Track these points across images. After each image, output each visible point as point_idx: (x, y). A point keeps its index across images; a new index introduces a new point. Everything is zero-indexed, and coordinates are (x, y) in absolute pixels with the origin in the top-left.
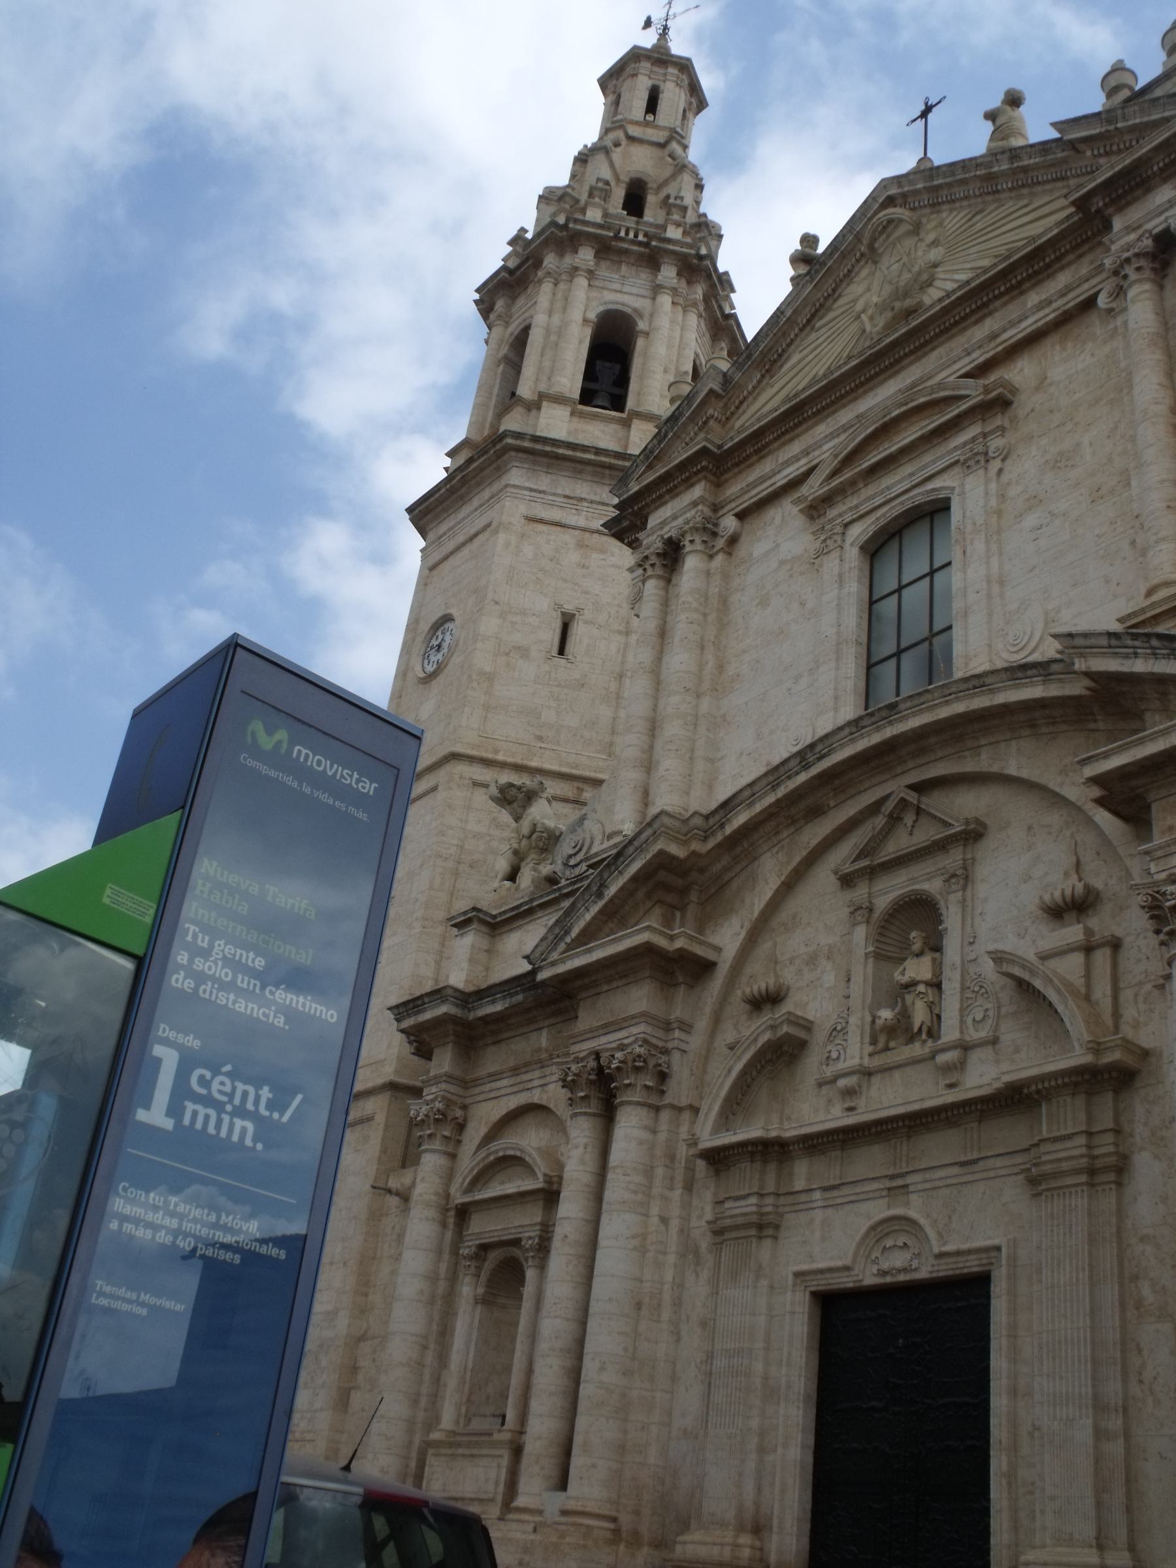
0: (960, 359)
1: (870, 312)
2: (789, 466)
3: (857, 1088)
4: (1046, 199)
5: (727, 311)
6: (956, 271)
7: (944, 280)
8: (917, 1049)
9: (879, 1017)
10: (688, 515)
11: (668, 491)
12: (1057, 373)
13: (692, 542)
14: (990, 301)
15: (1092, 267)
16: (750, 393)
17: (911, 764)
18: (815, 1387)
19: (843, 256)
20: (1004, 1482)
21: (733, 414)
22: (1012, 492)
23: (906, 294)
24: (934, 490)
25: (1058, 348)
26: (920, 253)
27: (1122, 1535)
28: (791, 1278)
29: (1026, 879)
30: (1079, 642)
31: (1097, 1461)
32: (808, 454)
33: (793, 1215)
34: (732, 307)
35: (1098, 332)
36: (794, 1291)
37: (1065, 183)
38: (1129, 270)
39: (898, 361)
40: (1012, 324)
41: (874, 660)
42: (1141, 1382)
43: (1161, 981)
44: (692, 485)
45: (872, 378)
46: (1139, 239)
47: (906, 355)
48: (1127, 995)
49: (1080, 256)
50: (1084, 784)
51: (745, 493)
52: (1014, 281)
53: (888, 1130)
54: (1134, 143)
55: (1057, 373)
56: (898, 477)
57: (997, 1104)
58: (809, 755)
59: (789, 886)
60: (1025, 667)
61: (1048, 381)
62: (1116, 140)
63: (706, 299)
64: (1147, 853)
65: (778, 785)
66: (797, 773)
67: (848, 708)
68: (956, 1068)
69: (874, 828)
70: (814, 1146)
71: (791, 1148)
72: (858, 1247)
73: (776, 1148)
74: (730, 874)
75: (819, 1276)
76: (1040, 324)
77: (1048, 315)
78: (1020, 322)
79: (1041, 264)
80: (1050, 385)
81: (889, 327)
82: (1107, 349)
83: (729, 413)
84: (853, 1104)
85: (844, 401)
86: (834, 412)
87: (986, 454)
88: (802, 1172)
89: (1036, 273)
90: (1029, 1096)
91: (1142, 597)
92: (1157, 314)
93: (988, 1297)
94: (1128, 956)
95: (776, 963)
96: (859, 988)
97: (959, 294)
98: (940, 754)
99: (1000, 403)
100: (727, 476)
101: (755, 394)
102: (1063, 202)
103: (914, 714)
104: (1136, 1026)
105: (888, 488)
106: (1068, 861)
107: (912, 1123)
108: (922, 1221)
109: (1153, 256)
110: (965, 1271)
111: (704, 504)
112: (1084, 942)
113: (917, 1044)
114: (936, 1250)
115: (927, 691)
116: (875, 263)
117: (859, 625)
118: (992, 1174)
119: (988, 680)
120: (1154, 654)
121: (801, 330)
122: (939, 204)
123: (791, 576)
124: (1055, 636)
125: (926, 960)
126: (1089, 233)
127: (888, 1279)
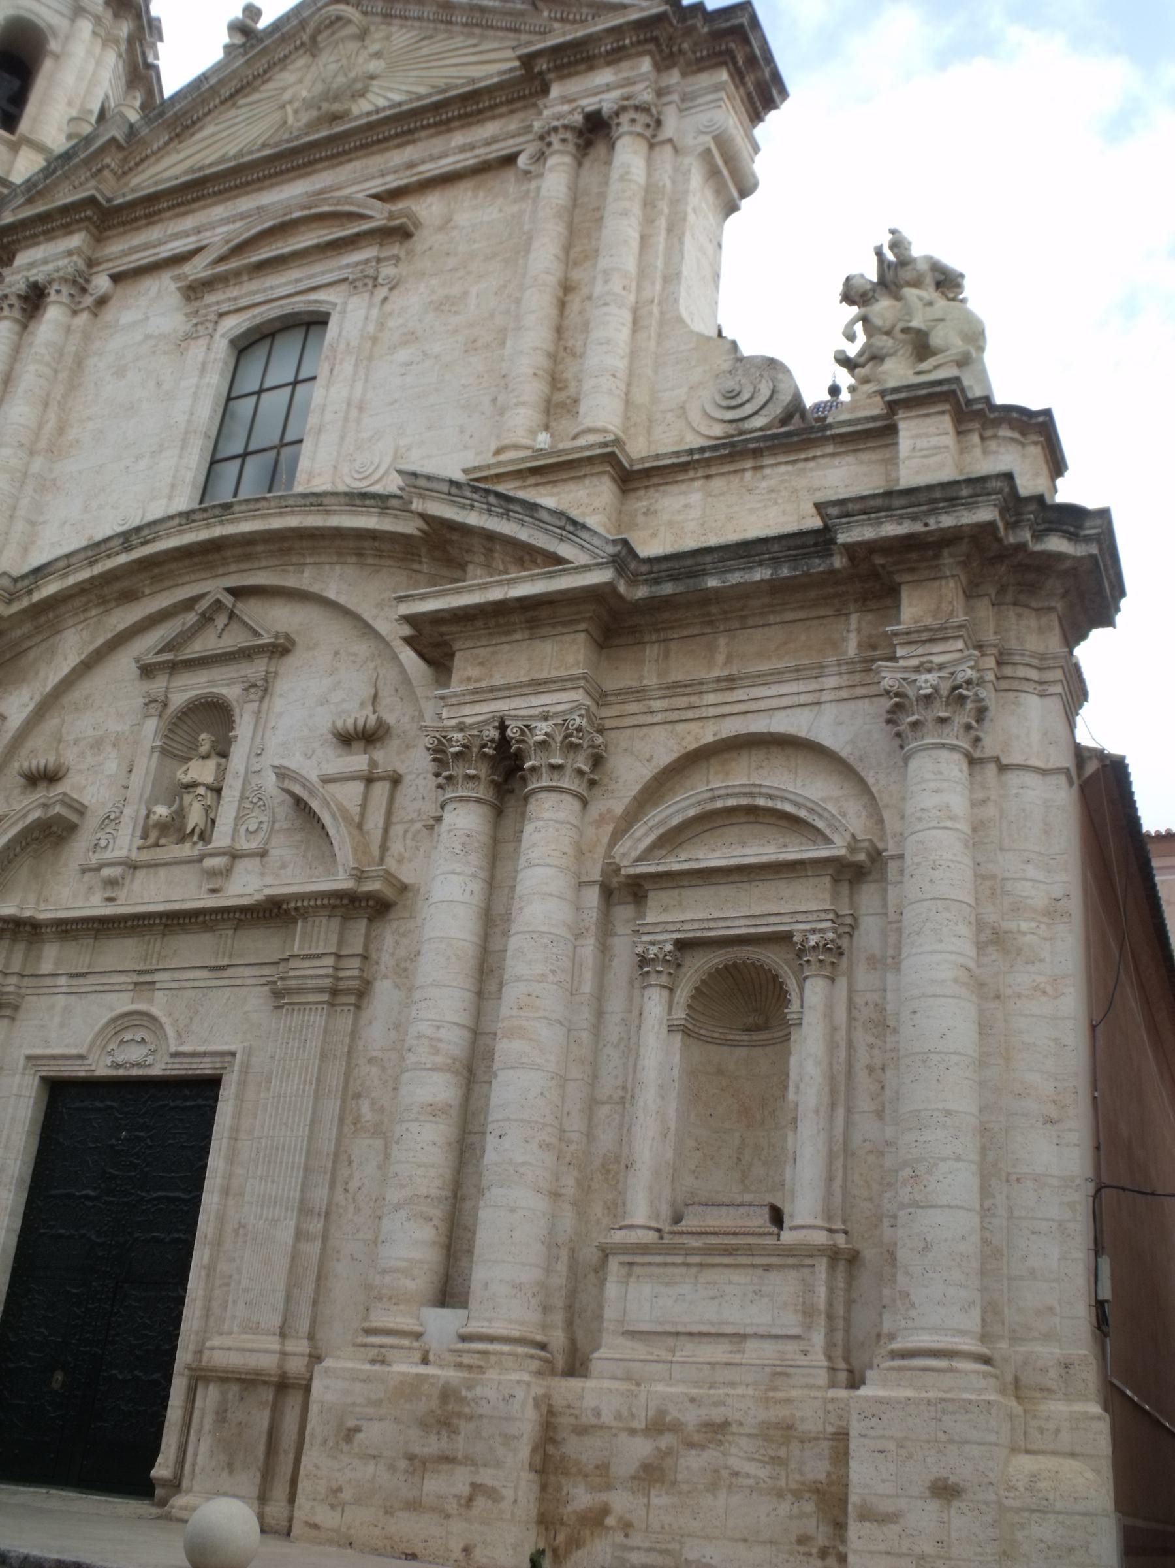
0: (373, 178)
1: (296, 105)
2: (177, 239)
3: (120, 880)
4: (496, 45)
5: (151, 59)
6: (391, 89)
7: (378, 95)
8: (187, 850)
9: (154, 813)
10: (61, 263)
11: (45, 233)
12: (463, 218)
13: (58, 292)
14: (416, 129)
15: (522, 125)
16: (153, 153)
17: (233, 568)
18: (30, 1171)
19: (284, 39)
20: (203, 1273)
21: (131, 169)
22: (391, 323)
23: (336, 98)
24: (316, 301)
25: (470, 194)
26: (360, 60)
27: (304, 1326)
28: (22, 1061)
29: (324, 701)
30: (422, 482)
31: (293, 1258)
32: (199, 232)
33: (35, 998)
34: (157, 57)
35: (511, 190)
36: (23, 1074)
37: (517, 36)
38: (554, 139)
39: (311, 163)
40: (432, 159)
41: (219, 456)
42: (346, 1190)
43: (432, 822)
44: (71, 233)
45: (282, 172)
46: (571, 112)
47: (321, 160)
48: (397, 830)
49: (512, 112)
50: (397, 620)
51: (126, 255)
52: (444, 117)
53: (138, 926)
54: (590, 18)
55: (463, 218)
56: (284, 280)
57: (255, 915)
58: (134, 537)
59: (87, 666)
60: (364, 496)
61: (452, 224)
62: (574, 10)
63: (131, 40)
64: (442, 698)
65: (96, 561)
66: (118, 554)
67: (182, 499)
68: (221, 873)
69: (184, 624)
70: (66, 931)
71: (43, 930)
72: (98, 1035)
73: (28, 928)
74: (30, 643)
75: (52, 1062)
76: (459, 166)
77: (468, 160)
78: (440, 158)
79: (474, 107)
80: (452, 228)
81: (313, 126)
82: (515, 208)
83: (126, 168)
84: (113, 895)
85: (248, 188)
86: (236, 197)
87: (376, 279)
88: (51, 956)
89: (467, 115)
90: (287, 912)
91: (491, 454)
92: (570, 188)
93: (216, 1100)
94: (406, 792)
95: (60, 741)
96: (140, 781)
97: (388, 113)
98: (264, 563)
99: (401, 233)
100: (109, 233)
101: (159, 155)
102: (510, 54)
103: (246, 519)
104: (400, 861)
105: (271, 288)
106: (367, 692)
107: (169, 922)
108: (164, 1019)
109: (580, 133)
110: (198, 1072)
111: (79, 255)
112: (366, 773)
113: (188, 845)
114: (173, 1049)
115: (264, 499)
116: (314, 56)
117: (211, 418)
118: (239, 982)
119: (326, 501)
120: (489, 511)
121: (222, 103)
122: (391, 16)
123: (154, 353)
124: (400, 472)
125: (211, 764)
126: (527, 92)
127: (121, 1072)
